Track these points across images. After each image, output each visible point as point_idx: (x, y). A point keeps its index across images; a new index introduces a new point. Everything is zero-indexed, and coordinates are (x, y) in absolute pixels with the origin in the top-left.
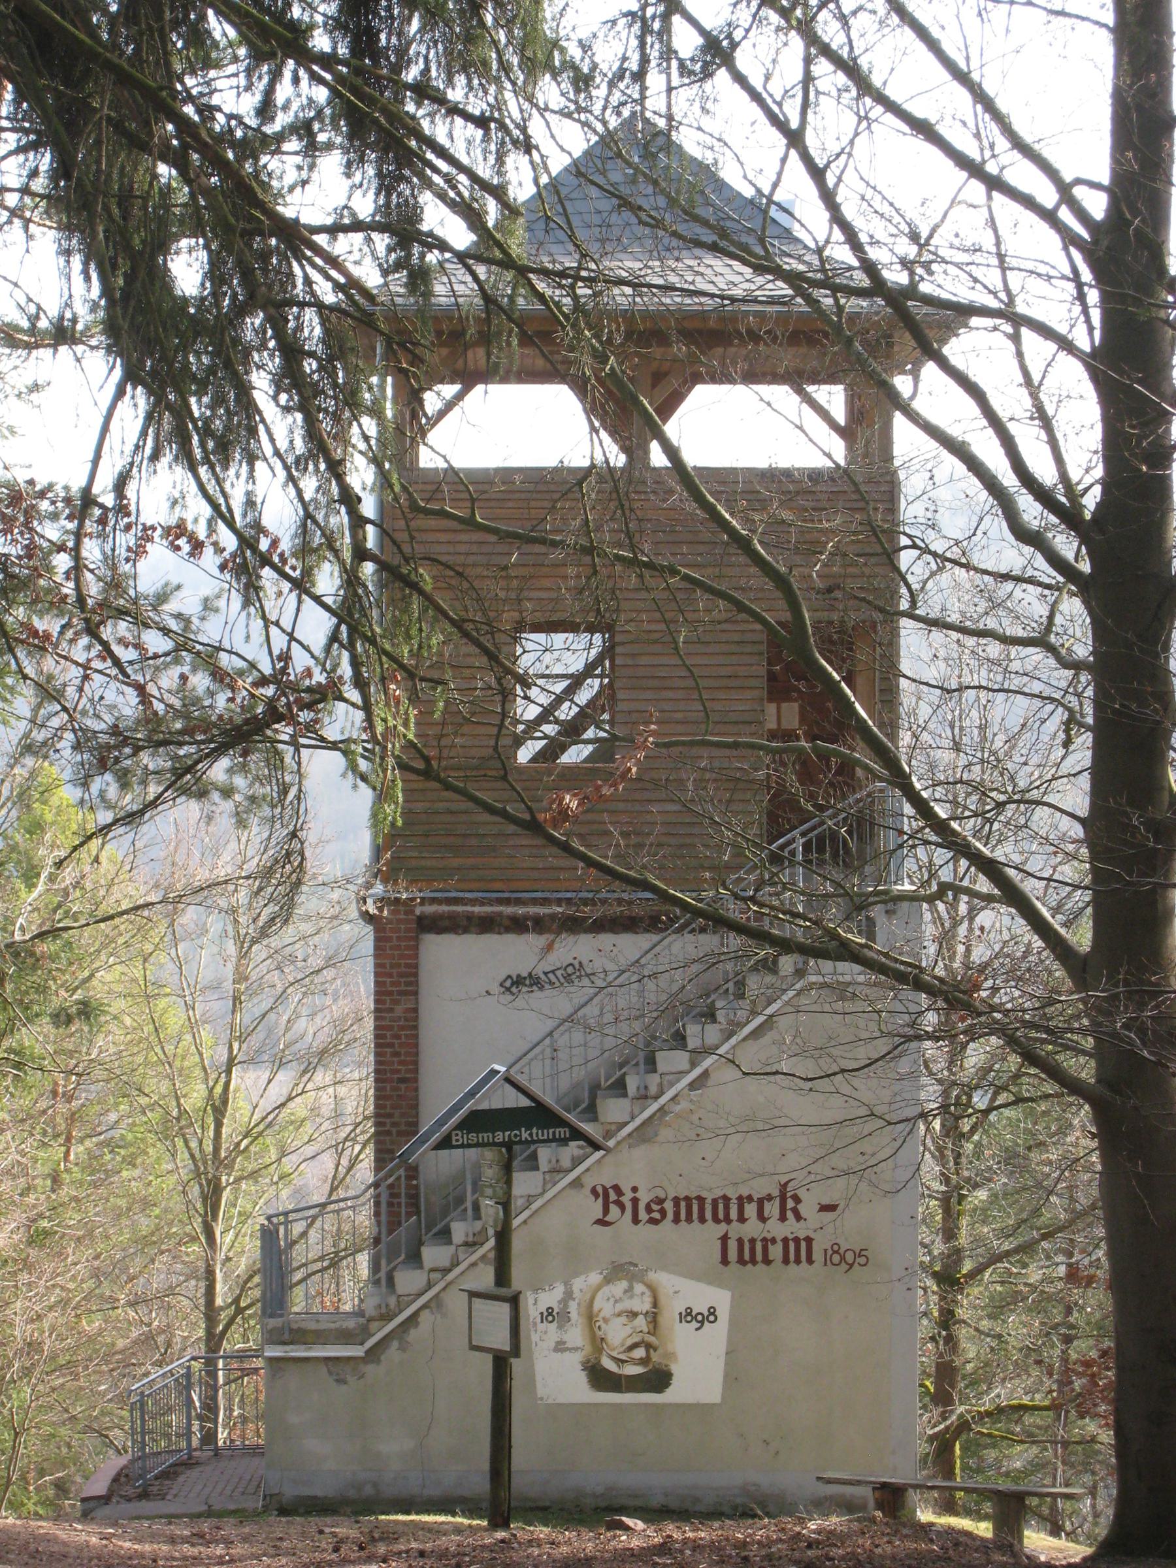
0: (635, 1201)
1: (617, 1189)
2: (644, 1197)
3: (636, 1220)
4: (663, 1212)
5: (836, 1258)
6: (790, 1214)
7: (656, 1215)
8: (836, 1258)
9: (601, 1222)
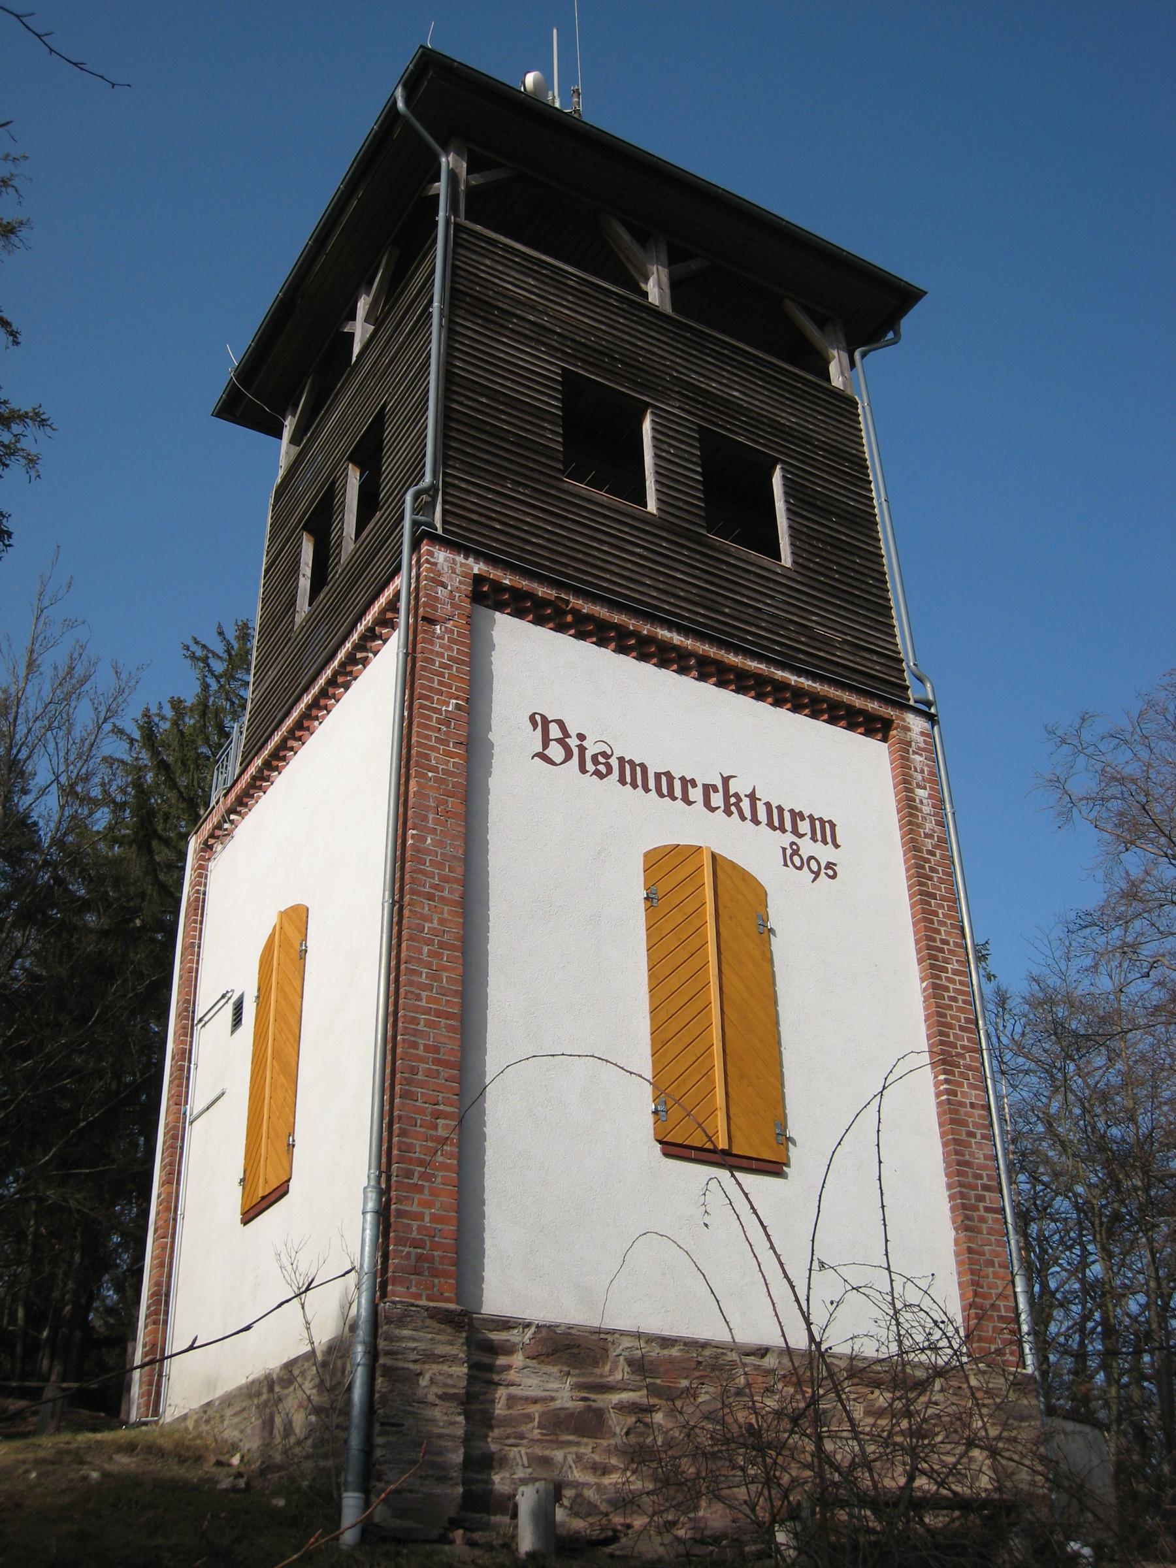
6: (733, 808)
7: (602, 768)
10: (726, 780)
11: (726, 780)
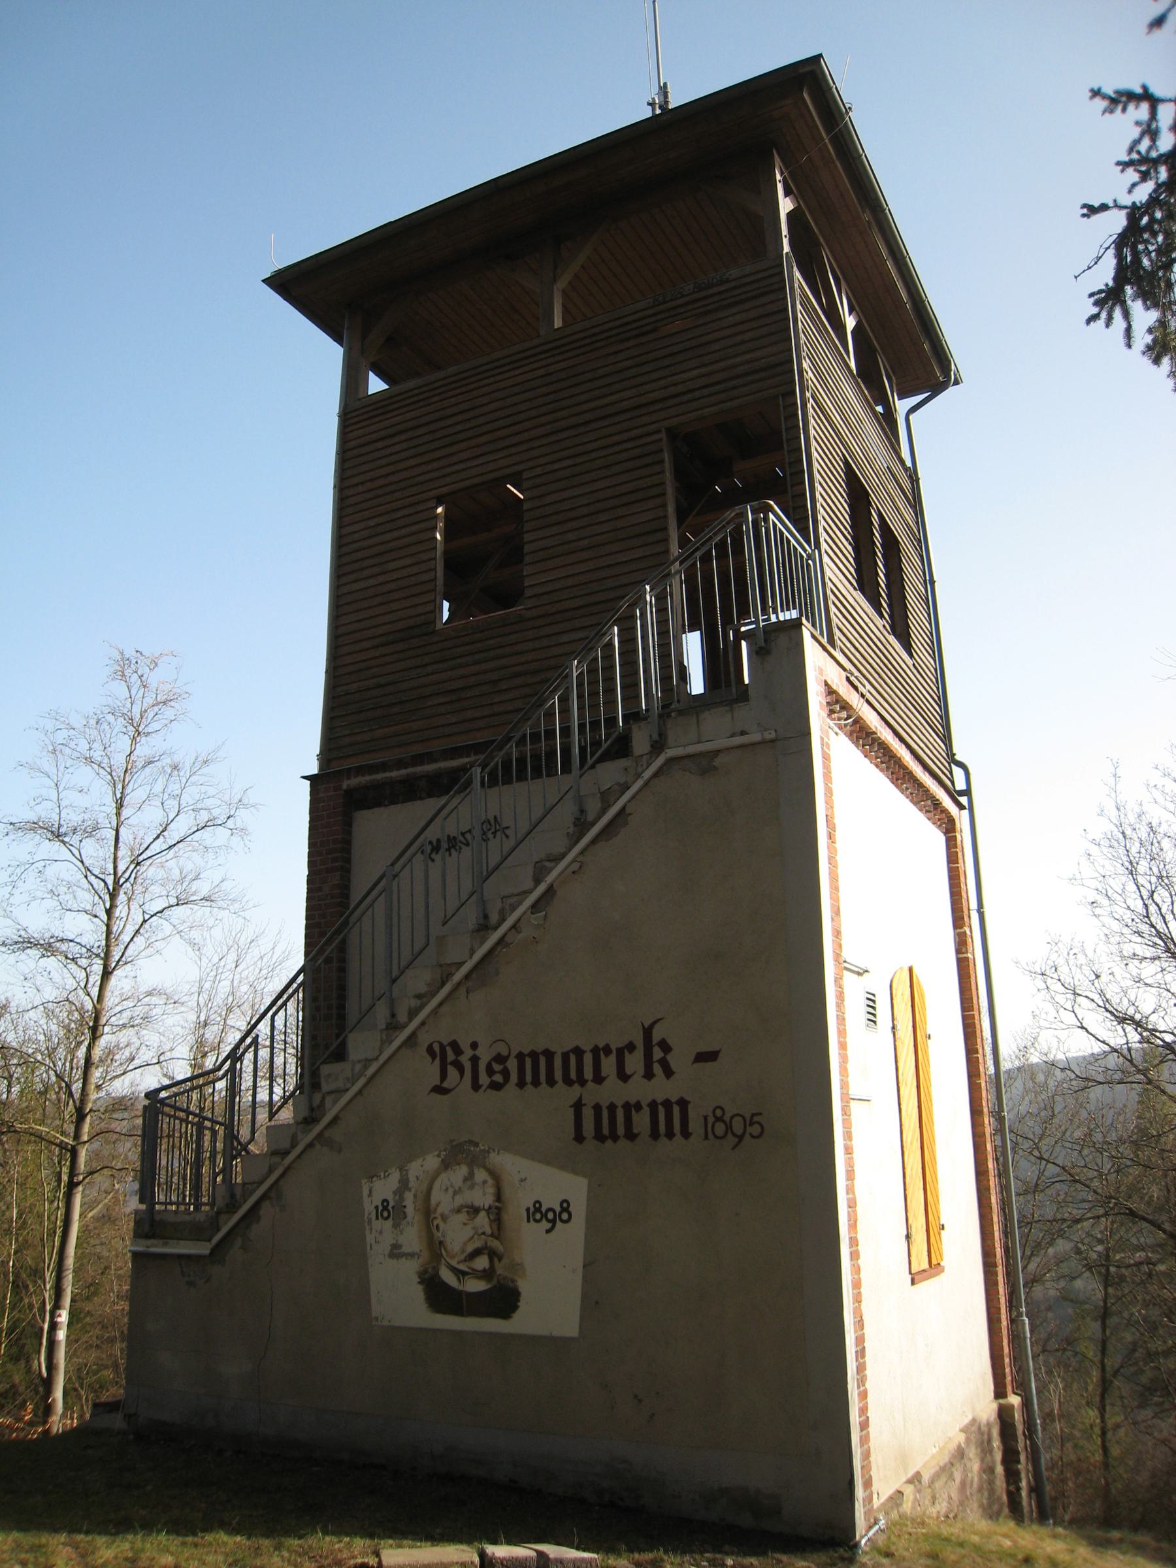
0: (475, 1060)
1: (455, 1045)
2: (485, 1055)
3: (476, 1086)
4: (506, 1074)
5: (538, 1216)
6: (657, 1069)
8: (538, 1216)
9: (439, 1090)
10: (648, 1032)
11: (648, 1032)
